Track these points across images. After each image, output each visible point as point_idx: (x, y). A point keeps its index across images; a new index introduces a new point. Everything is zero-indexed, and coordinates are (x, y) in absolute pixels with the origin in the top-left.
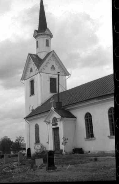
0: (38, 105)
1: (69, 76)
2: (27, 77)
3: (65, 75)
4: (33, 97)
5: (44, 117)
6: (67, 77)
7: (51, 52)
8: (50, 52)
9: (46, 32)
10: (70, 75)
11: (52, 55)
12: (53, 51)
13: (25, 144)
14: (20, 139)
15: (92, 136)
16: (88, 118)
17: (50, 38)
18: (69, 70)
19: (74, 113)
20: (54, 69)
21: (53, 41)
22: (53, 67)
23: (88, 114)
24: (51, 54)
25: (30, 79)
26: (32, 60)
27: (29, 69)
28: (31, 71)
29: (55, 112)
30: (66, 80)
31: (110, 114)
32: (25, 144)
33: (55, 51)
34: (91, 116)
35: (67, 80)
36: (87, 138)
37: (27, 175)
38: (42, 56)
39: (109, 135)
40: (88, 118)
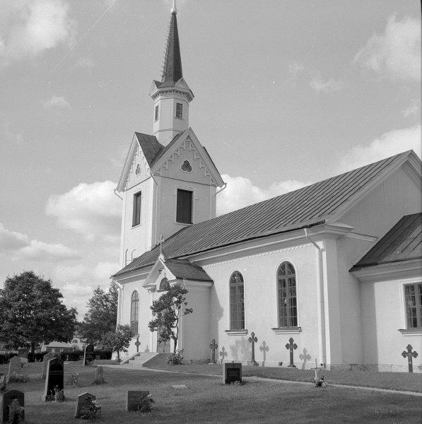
1: (224, 186)
2: (129, 185)
3: (212, 185)
4: (137, 228)
5: (144, 277)
6: (218, 188)
9: (179, 85)
11: (184, 136)
12: (190, 129)
13: (130, 393)
14: (74, 311)
15: (294, 322)
16: (237, 281)
18: (224, 177)
19: (210, 270)
20: (190, 169)
22: (187, 166)
24: (183, 138)
25: (136, 190)
26: (140, 147)
27: (134, 167)
28: (138, 171)
31: (282, 277)
32: (130, 393)
34: (243, 281)
38: (164, 140)
39: (404, 327)
40: (237, 281)
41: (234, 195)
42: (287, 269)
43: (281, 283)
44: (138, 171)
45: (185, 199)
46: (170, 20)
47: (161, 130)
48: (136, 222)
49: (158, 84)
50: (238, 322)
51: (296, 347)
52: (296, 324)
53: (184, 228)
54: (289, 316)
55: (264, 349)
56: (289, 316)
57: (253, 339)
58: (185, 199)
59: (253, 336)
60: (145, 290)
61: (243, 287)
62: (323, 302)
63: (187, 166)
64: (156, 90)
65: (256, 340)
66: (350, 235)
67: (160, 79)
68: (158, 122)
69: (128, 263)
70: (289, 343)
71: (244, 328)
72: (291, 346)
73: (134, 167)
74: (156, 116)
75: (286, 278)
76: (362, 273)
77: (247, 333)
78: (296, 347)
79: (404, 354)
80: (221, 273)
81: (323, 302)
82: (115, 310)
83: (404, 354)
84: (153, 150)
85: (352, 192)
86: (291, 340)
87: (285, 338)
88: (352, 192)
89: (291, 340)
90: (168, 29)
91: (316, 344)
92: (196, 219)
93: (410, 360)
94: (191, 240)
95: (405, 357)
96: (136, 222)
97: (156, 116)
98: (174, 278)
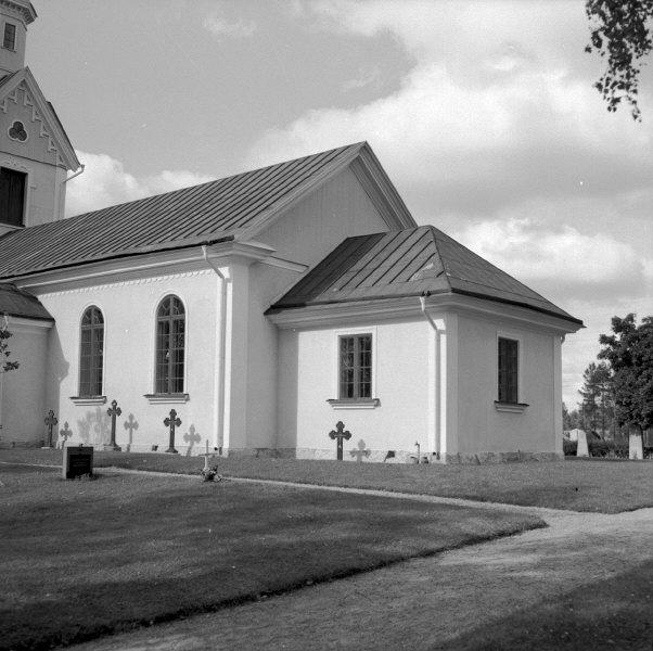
1: (79, 170)
6: (71, 173)
10: (83, 166)
12: (27, 70)
16: (93, 323)
31: (165, 319)
34: (102, 322)
40: (93, 323)
42: (93, 316)
43: (163, 328)
50: (92, 383)
51: (179, 422)
52: (181, 389)
54: (171, 376)
55: (131, 425)
56: (171, 376)
57: (115, 411)
61: (102, 330)
62: (223, 358)
66: (270, 261)
78: (179, 422)
81: (223, 358)
87: (163, 409)
89: (173, 413)
91: (209, 420)
93: (340, 443)
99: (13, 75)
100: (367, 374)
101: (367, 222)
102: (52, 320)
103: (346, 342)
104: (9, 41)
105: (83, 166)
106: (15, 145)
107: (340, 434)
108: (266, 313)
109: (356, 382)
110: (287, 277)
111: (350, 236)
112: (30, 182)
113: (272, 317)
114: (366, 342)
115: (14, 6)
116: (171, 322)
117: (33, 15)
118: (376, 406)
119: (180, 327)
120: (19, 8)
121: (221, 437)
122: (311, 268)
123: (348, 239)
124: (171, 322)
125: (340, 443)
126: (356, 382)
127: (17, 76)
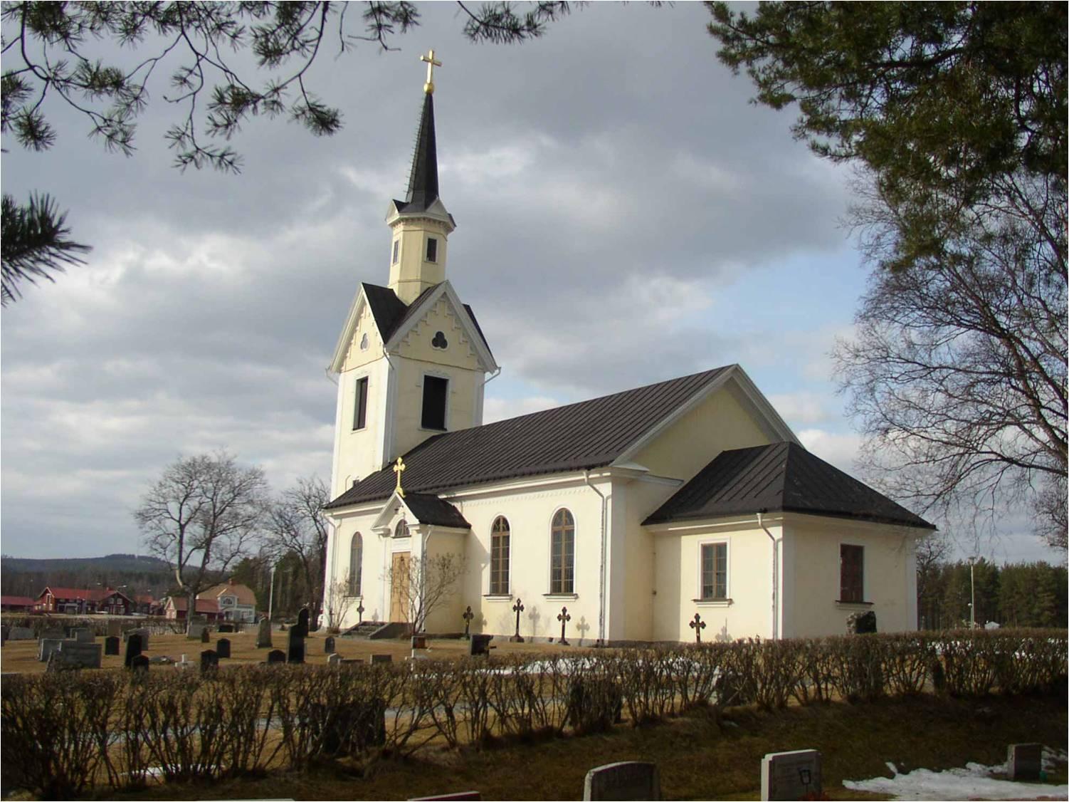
0: (453, 393)
1: (497, 371)
2: (349, 363)
6: (488, 375)
7: (436, 286)
8: (437, 283)
9: (432, 211)
10: (500, 368)
12: (447, 282)
16: (501, 526)
17: (442, 232)
21: (452, 245)
22: (439, 341)
23: (501, 521)
24: (437, 294)
28: (364, 344)
29: (403, 503)
30: (483, 385)
31: (557, 528)
33: (452, 283)
34: (508, 529)
35: (486, 385)
36: (841, 602)
37: (302, 693)
38: (408, 295)
40: (501, 526)
41: (503, 400)
42: (564, 518)
43: (556, 535)
44: (364, 344)
45: (435, 391)
46: (423, 102)
47: (400, 280)
48: (360, 422)
49: (400, 206)
50: (500, 586)
51: (569, 618)
52: (572, 590)
53: (433, 439)
54: (562, 582)
55: (534, 617)
56: (562, 582)
57: (518, 608)
58: (435, 391)
59: (519, 604)
60: (374, 535)
61: (508, 537)
63: (439, 341)
64: (396, 215)
65: (522, 608)
67: (402, 199)
68: (394, 240)
69: (348, 489)
70: (562, 614)
71: (507, 592)
72: (564, 617)
73: (358, 338)
74: (395, 256)
75: (563, 528)
76: (655, 528)
77: (511, 599)
78: (569, 618)
79: (692, 625)
80: (479, 511)
82: (323, 553)
83: (692, 625)
84: (391, 314)
85: (652, 421)
86: (564, 610)
87: (558, 604)
88: (652, 421)
89: (564, 610)
90: (419, 117)
91: (590, 614)
92: (454, 422)
93: (698, 631)
94: (441, 461)
95: (703, 623)
96: (360, 422)
97: (395, 256)
98: (417, 521)
99: (436, 286)
100: (722, 576)
101: (743, 436)
102: (468, 526)
103: (706, 549)
104: (103, 13)
105: (500, 368)
106: (438, 354)
107: (698, 624)
108: (644, 524)
109: (714, 588)
110: (661, 493)
111: (726, 450)
112: (450, 388)
113: (648, 527)
114: (721, 549)
115: (435, 221)
116: (563, 526)
117: (451, 225)
118: (729, 604)
119: (570, 535)
120: (440, 222)
121: (602, 631)
122: (687, 482)
123: (724, 455)
124: (563, 526)
125: (698, 631)
126: (714, 588)
127: (440, 287)
